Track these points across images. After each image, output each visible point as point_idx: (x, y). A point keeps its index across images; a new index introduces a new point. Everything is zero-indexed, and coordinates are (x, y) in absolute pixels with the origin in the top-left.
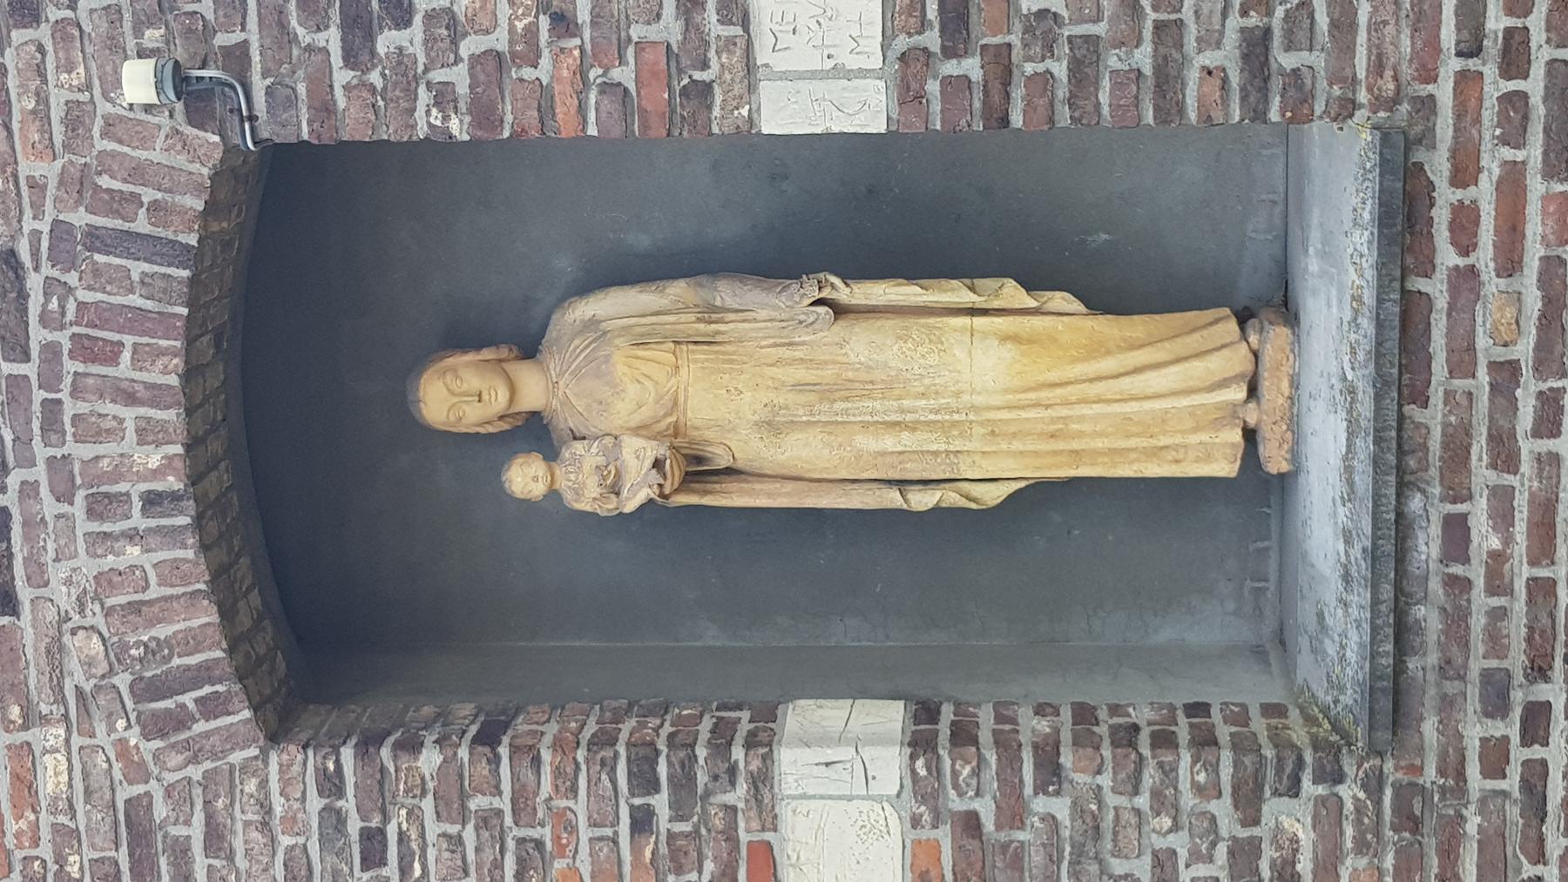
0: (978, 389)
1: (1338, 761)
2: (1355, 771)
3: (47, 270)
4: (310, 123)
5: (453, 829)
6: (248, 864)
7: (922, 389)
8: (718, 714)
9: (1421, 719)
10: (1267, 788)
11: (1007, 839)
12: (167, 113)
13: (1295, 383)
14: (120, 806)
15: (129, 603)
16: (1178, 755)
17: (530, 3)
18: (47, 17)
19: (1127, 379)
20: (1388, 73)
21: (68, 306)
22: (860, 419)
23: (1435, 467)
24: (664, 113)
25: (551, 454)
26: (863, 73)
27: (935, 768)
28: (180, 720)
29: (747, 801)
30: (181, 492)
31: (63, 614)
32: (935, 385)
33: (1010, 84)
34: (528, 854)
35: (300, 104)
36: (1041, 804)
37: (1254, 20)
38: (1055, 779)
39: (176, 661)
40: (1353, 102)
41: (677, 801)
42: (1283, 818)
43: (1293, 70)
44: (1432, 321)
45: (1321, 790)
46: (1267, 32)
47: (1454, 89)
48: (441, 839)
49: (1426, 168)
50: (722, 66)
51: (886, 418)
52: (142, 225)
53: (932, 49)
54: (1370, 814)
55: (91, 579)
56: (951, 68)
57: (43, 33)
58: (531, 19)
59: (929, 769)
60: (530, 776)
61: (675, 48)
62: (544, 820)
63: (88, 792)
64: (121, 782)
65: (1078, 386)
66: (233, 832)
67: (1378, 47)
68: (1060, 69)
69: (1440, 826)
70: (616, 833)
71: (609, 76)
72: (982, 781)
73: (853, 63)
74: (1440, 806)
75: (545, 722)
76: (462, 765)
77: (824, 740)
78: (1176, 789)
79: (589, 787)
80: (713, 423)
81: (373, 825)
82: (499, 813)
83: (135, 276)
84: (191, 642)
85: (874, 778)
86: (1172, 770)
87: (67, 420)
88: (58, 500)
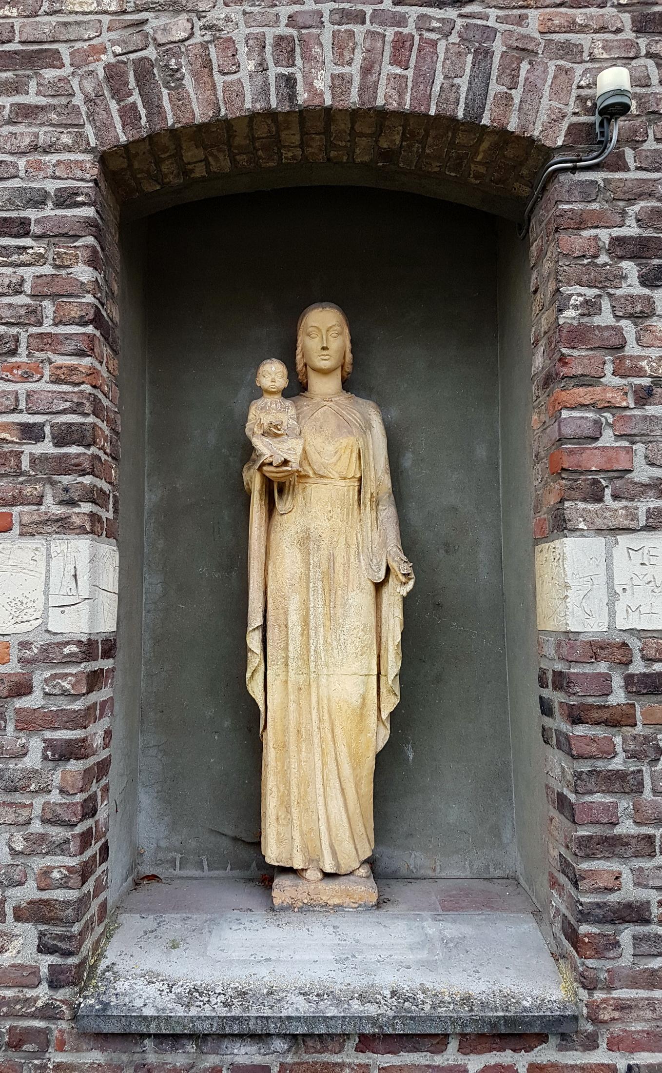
0: (330, 679)
1: (68, 984)
2: (60, 998)
3: (460, 22)
4: (571, 210)
5: (27, 288)
6: (4, 134)
7: (329, 640)
8: (111, 495)
9: (103, 1051)
10: (46, 927)
11: (8, 717)
12: (577, 111)
13: (338, 908)
14: (54, 46)
15: (211, 60)
16: (75, 856)
17: (660, 371)
18: (640, 37)
19: (338, 785)
20: (616, 1014)
21: (434, 34)
22: (311, 599)
23: (308, 1059)
24: (580, 466)
25: (287, 393)
26: (612, 614)
27: (69, 661)
28: (119, 93)
29: (46, 513)
30: (295, 102)
31: (204, 14)
32: (332, 649)
33: (606, 725)
34: (5, 343)
35: (584, 204)
36: (36, 745)
37: (655, 911)
38: (57, 756)
39: (165, 92)
40: (595, 988)
41: (47, 459)
42: (21, 940)
43: (618, 942)
44: (425, 1053)
45: (44, 971)
46: (647, 922)
47: (603, 1064)
48: (19, 278)
49: (544, 1045)
50: (616, 510)
51: (312, 616)
52: (494, 88)
53: (631, 667)
54: (24, 1010)
55: (230, 35)
56: (617, 681)
57: (628, 34)
58: (649, 371)
59: (69, 655)
60: (70, 347)
61: (629, 476)
62: (33, 356)
63: (66, 24)
64: (73, 47)
65: (333, 750)
66: (30, 125)
67: (636, 1006)
68: (617, 764)
69: (13, 1065)
70: (21, 412)
71: (607, 427)
72: (58, 697)
73: (620, 607)
74: (30, 1065)
75: (108, 368)
76: (78, 296)
77: (94, 573)
78: (47, 854)
79: (59, 392)
80: (308, 501)
81: (32, 228)
82: (40, 324)
83: (457, 81)
84: (180, 101)
85: (63, 612)
86: (62, 850)
87: (350, 27)
88: (290, 17)
